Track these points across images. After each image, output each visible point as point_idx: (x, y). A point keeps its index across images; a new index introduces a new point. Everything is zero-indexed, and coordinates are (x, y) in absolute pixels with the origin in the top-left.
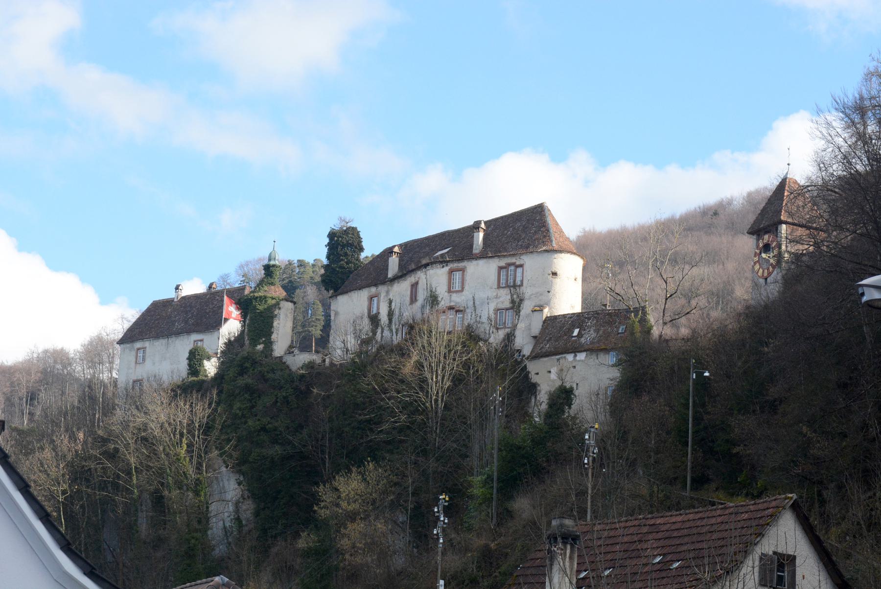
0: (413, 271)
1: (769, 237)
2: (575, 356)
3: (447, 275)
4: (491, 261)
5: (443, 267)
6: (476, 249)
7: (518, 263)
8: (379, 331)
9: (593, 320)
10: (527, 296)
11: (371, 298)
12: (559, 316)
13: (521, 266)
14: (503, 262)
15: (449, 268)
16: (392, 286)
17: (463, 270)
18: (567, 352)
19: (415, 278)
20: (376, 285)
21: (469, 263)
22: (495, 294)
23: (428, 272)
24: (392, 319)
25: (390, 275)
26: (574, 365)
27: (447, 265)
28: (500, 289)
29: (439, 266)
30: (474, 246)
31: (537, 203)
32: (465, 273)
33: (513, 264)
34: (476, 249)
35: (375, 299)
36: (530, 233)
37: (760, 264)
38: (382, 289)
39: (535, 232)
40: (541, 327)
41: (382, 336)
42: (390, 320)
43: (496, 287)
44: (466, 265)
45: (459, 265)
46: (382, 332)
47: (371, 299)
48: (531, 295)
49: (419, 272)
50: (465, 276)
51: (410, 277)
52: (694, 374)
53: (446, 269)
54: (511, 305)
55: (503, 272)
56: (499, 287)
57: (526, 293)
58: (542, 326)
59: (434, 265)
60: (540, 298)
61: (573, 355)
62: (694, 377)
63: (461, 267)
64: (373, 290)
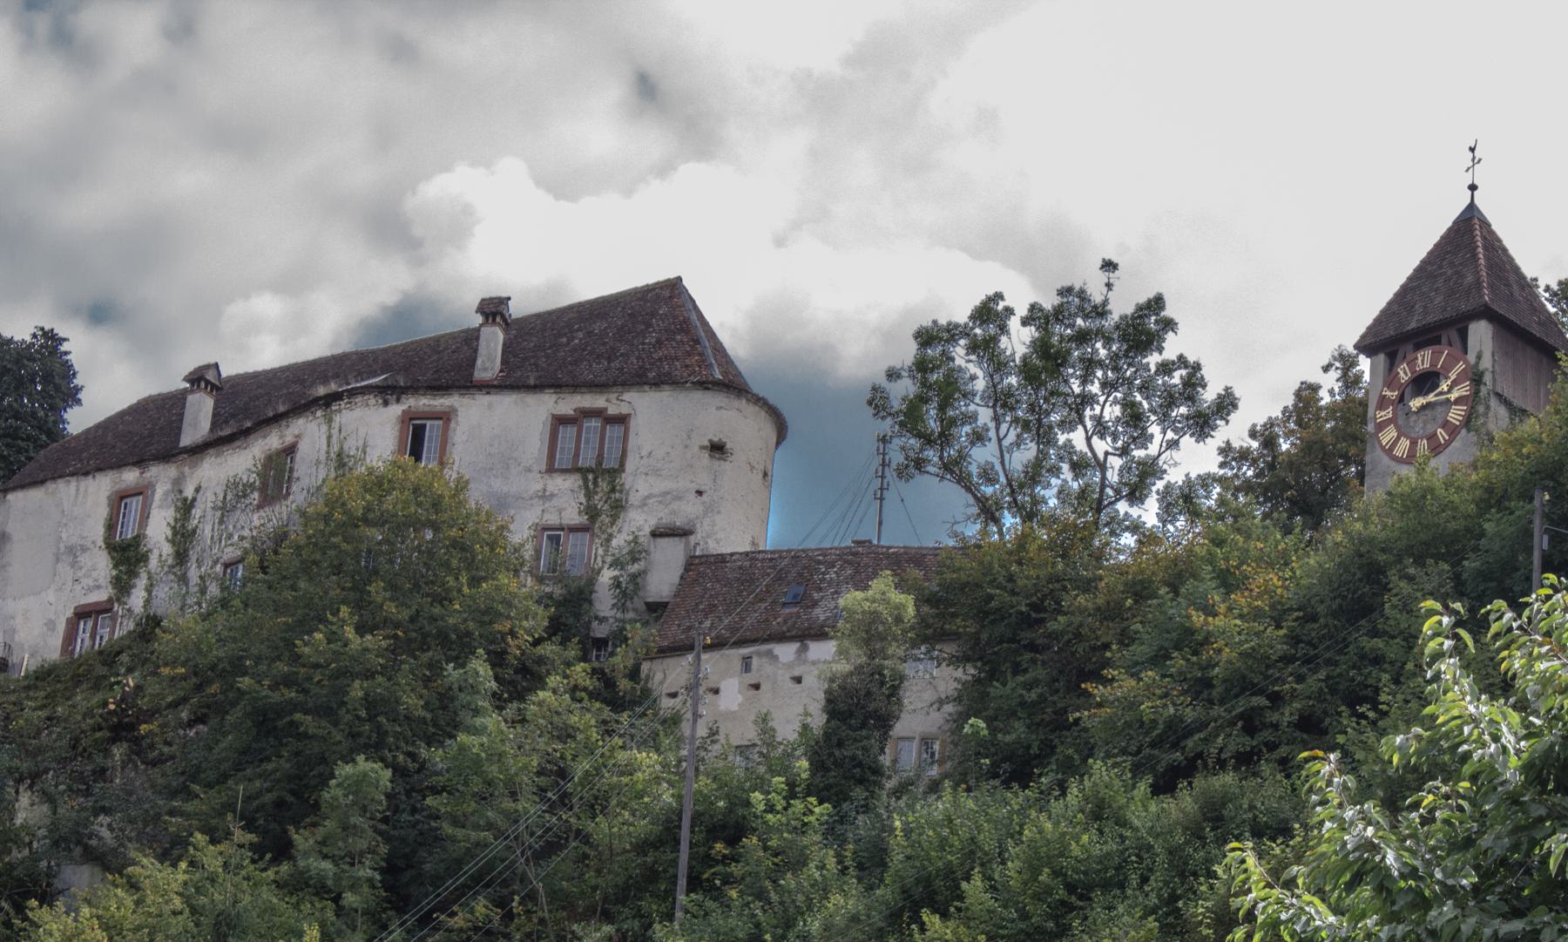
0: (277, 419)
1: (1436, 356)
2: (804, 649)
3: (398, 427)
4: (531, 399)
5: (386, 403)
6: (485, 369)
7: (612, 410)
8: (142, 582)
9: (842, 568)
10: (634, 499)
11: (122, 498)
12: (732, 555)
13: (622, 420)
14: (568, 404)
15: (405, 407)
16: (193, 466)
17: (446, 417)
18: (782, 638)
19: (281, 437)
20: (141, 462)
21: (466, 400)
22: (539, 487)
23: (337, 418)
24: (186, 550)
25: (186, 440)
26: (796, 673)
27: (398, 401)
28: (555, 475)
29: (372, 401)
30: (479, 362)
31: (662, 277)
32: (452, 425)
33: (597, 413)
34: (485, 369)
35: (135, 503)
36: (643, 343)
37: (1398, 428)
38: (161, 476)
39: (659, 342)
40: (677, 580)
41: (148, 602)
42: (181, 557)
43: (544, 468)
44: (456, 405)
45: (433, 402)
46: (149, 589)
47: (120, 499)
48: (648, 497)
49: (301, 421)
50: (451, 433)
51: (265, 437)
52: (1546, 538)
53: (396, 410)
54: (584, 519)
55: (567, 433)
56: (551, 469)
57: (632, 494)
58: (682, 578)
59: (359, 399)
60: (675, 506)
61: (794, 646)
62: (1545, 546)
63: (439, 409)
64: (130, 476)
